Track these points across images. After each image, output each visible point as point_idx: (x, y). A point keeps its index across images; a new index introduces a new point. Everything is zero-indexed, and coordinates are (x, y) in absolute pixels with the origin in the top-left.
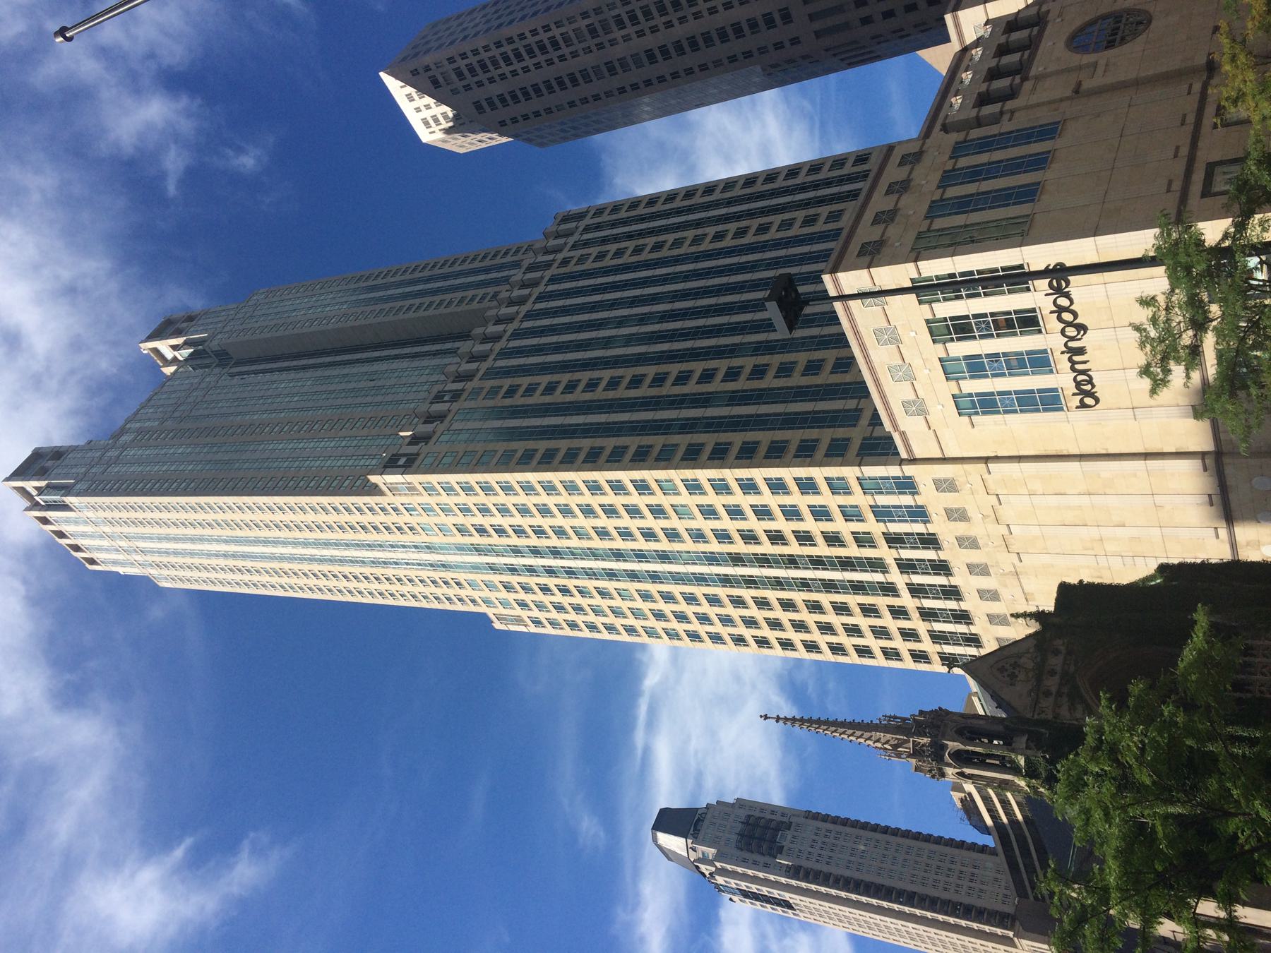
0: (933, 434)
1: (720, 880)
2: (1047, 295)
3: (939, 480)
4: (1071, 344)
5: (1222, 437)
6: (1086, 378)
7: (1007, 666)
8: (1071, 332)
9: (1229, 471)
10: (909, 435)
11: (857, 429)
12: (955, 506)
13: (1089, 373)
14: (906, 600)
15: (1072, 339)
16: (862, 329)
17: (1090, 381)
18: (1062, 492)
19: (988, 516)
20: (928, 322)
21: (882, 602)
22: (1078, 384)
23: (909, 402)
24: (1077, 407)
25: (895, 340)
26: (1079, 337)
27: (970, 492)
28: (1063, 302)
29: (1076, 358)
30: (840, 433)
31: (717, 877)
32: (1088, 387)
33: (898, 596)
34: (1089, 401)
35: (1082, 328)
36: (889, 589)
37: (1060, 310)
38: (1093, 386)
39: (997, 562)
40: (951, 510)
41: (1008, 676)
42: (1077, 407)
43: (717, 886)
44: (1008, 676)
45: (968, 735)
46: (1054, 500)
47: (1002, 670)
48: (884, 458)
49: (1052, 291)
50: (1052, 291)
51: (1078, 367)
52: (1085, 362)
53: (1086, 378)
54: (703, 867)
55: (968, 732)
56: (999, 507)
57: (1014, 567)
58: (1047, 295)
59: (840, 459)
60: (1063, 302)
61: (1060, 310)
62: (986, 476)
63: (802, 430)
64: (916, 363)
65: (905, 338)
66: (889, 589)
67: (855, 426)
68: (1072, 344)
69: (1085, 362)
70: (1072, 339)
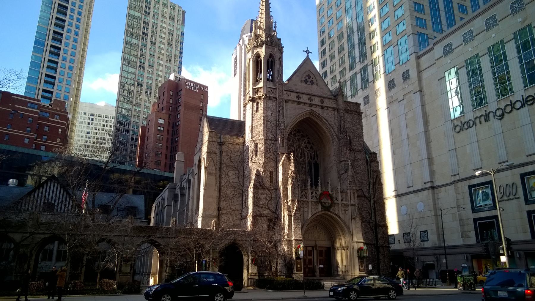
0: (434, 63)
1: (238, 48)
2: (522, 96)
3: (408, 72)
4: (491, 115)
5: (443, 189)
6: (471, 125)
7: (311, 79)
8: (499, 113)
9: (425, 192)
10: (432, 52)
11: (432, 32)
12: (396, 83)
13: (474, 126)
14: (349, 74)
15: (495, 114)
16: (495, 8)
17: (469, 127)
18: (408, 127)
19: (392, 99)
20: (502, 41)
21: (347, 65)
22: (468, 122)
23: (451, 45)
24: (454, 124)
25: (489, 27)
26: (496, 117)
27: (404, 87)
28: (518, 105)
29: (483, 118)
30: (429, 24)
31: (239, 46)
32: (466, 127)
33: (350, 71)
34: (458, 129)
35: (502, 116)
36: (352, 66)
37: (513, 105)
38: (467, 129)
39: (371, 107)
40: (394, 82)
41: (306, 79)
42: (454, 124)
43: (236, 48)
44: (306, 79)
45: (270, 60)
46: (403, 124)
47: (309, 76)
48: (418, 44)
49: (524, 99)
50: (524, 99)
51: (478, 120)
52: (480, 123)
53: (471, 125)
54: (241, 41)
55: (272, 60)
56: (397, 102)
57: (369, 115)
58: (522, 96)
59: (415, 24)
60: (518, 105)
61: (513, 105)
62: (413, 92)
63: (429, 6)
64: (475, 43)
65: (490, 32)
66: (352, 66)
67: (434, 30)
68: (491, 115)
69: (480, 123)
70: (495, 114)
